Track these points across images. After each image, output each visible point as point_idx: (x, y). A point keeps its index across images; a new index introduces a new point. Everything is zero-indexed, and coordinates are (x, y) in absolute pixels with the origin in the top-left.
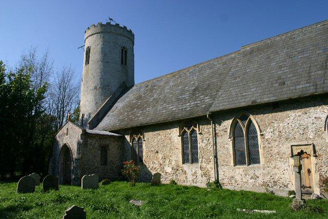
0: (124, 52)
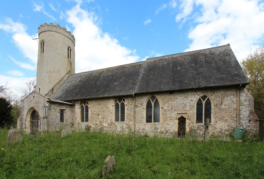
0: (69, 50)
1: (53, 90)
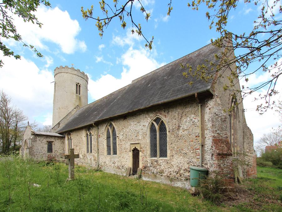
1: (59, 124)
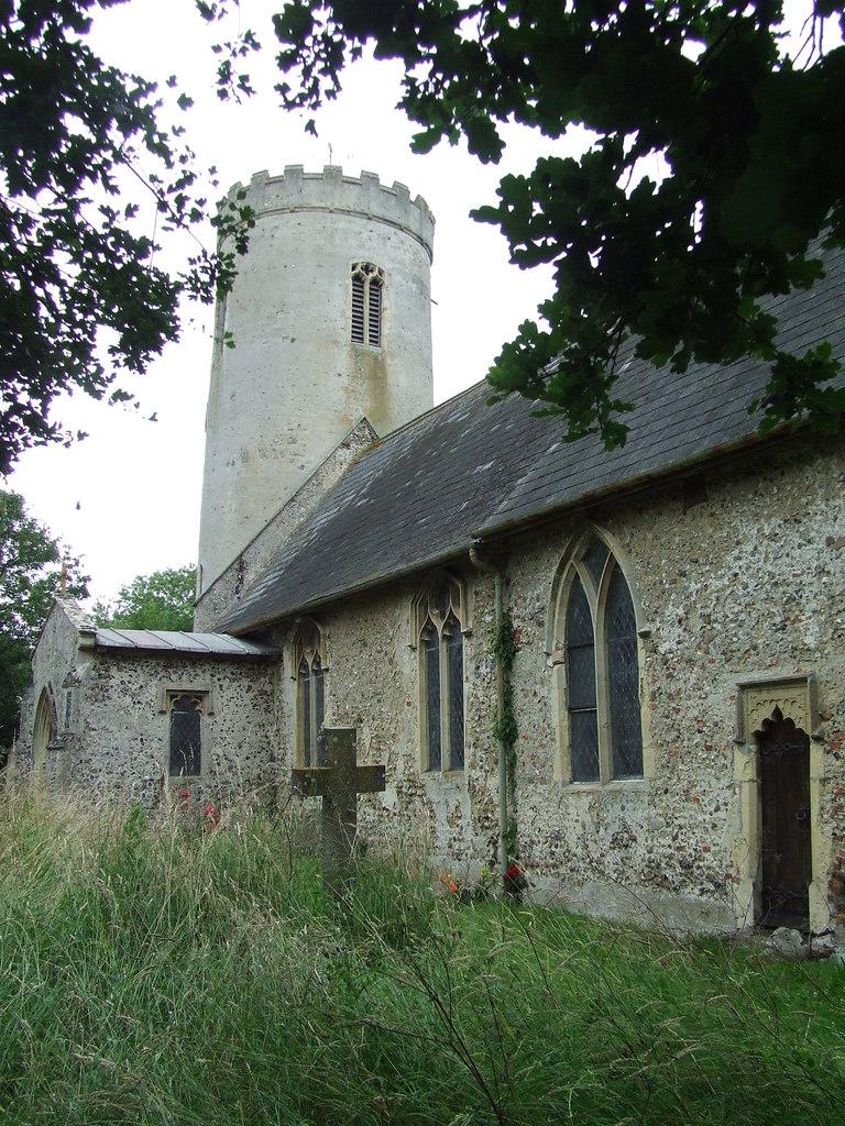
1: (241, 569)
